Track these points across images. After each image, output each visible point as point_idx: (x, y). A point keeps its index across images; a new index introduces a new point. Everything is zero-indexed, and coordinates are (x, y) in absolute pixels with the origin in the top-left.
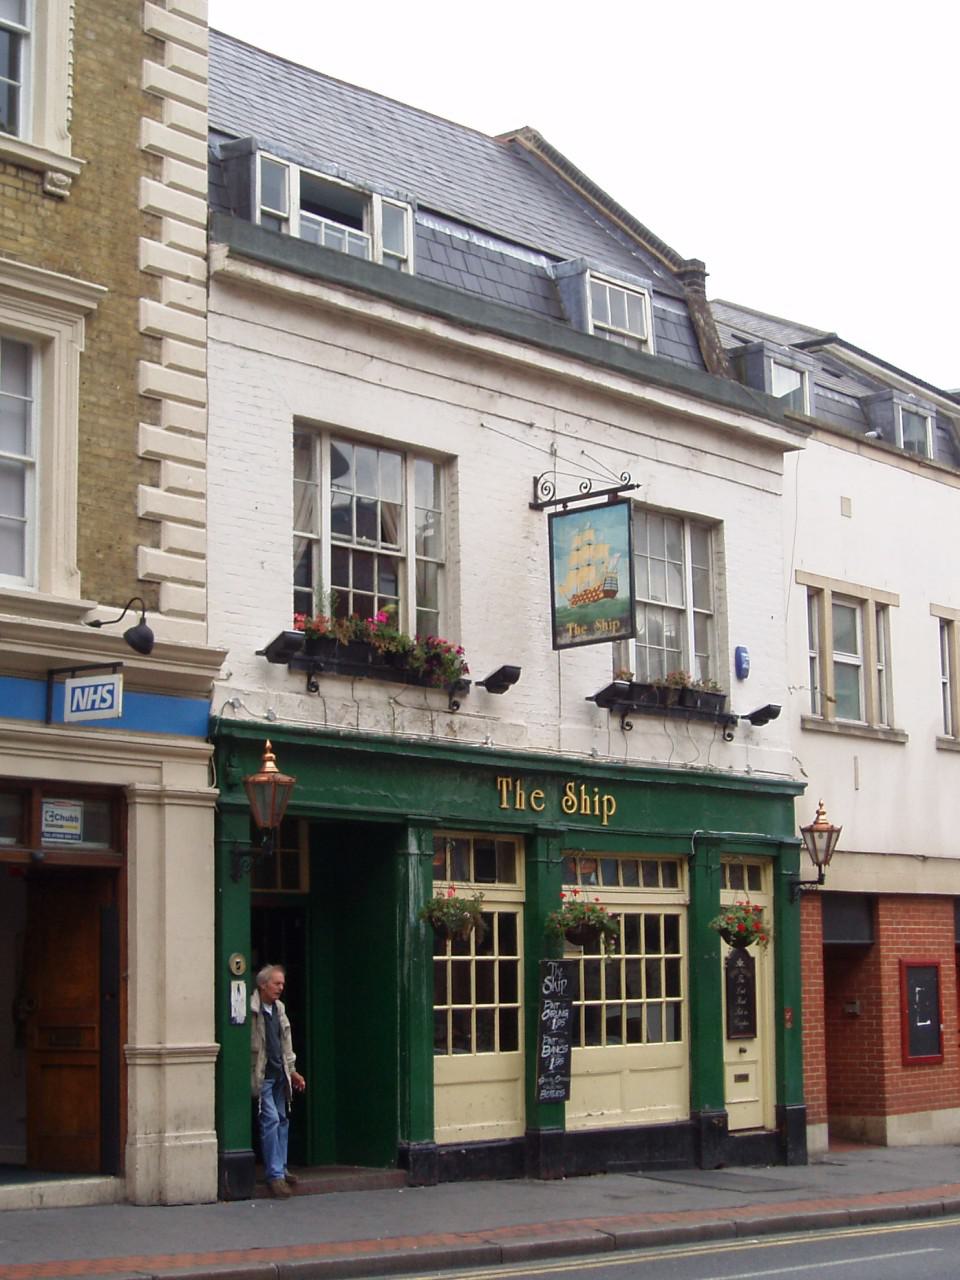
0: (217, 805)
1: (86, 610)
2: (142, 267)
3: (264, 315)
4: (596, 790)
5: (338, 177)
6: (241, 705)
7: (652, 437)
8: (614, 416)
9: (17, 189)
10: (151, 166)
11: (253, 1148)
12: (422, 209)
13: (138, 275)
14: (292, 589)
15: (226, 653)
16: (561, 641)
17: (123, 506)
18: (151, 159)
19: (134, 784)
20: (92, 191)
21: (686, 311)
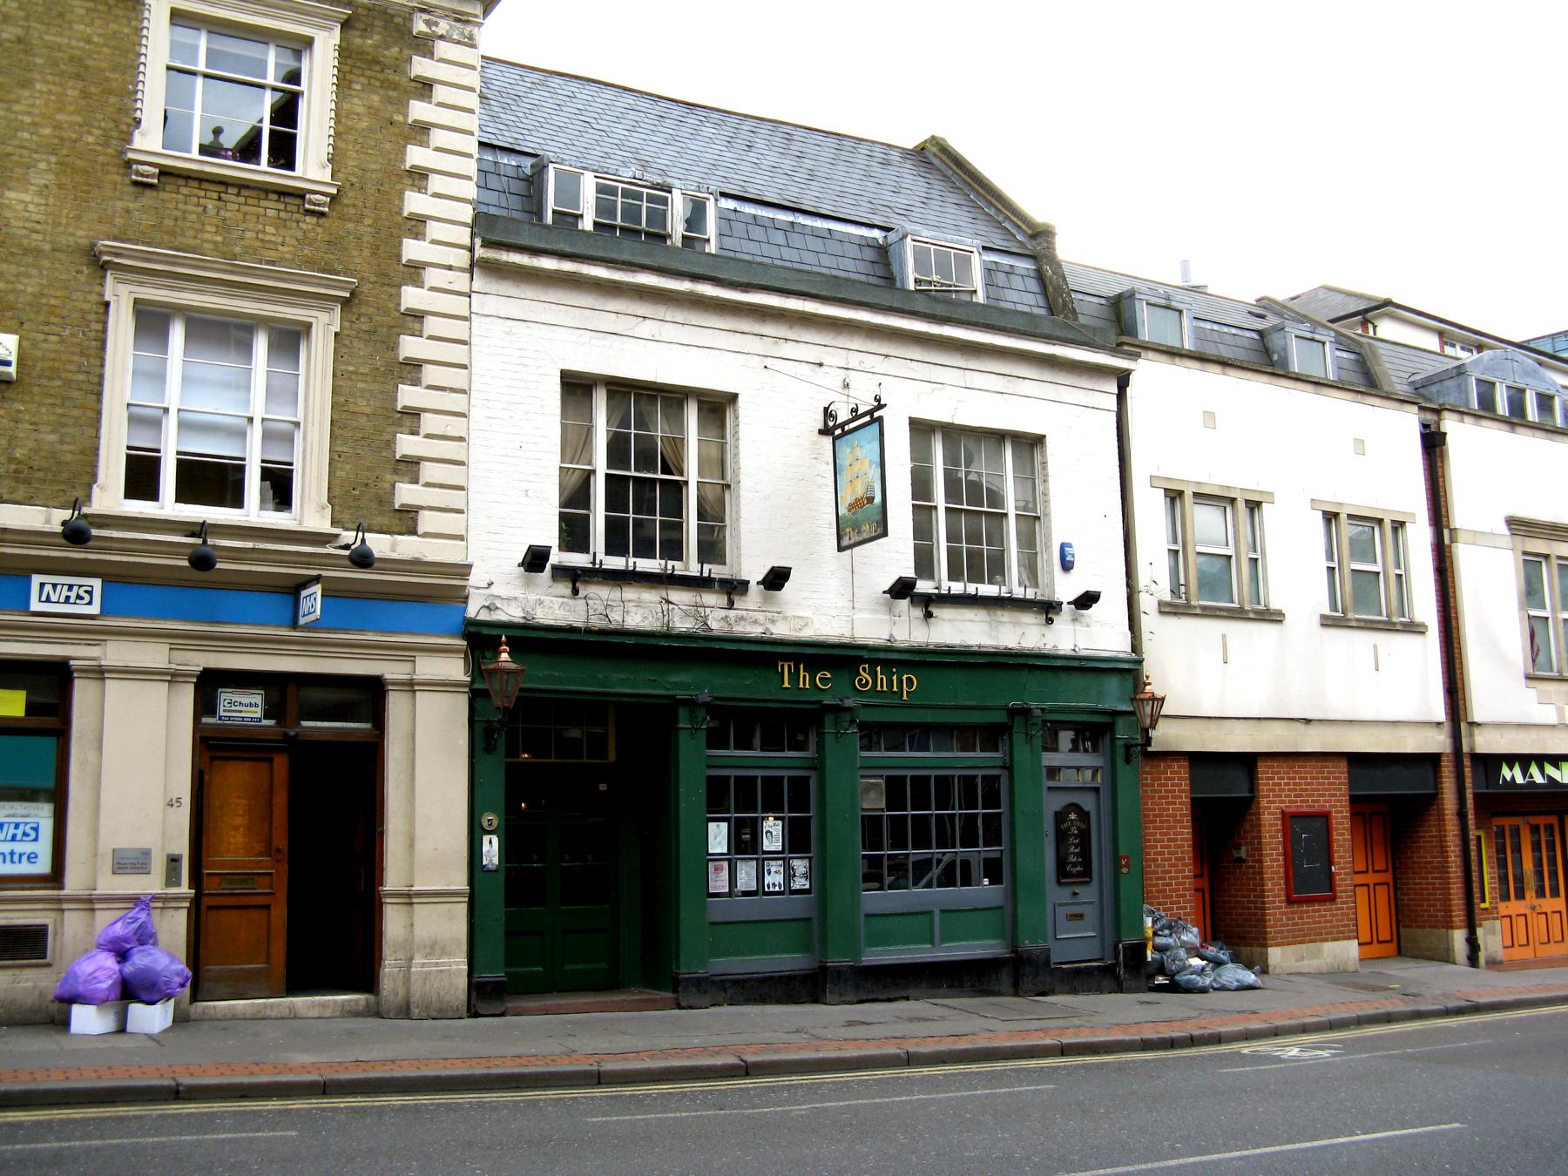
1: (337, 536)
2: (404, 262)
3: (529, 292)
5: (634, 178)
6: (497, 608)
8: (916, 353)
9: (279, 210)
10: (416, 182)
12: (723, 195)
13: (401, 268)
14: (556, 511)
16: (846, 542)
17: (380, 452)
18: (417, 176)
19: (383, 675)
20: (355, 206)
21: (1035, 265)
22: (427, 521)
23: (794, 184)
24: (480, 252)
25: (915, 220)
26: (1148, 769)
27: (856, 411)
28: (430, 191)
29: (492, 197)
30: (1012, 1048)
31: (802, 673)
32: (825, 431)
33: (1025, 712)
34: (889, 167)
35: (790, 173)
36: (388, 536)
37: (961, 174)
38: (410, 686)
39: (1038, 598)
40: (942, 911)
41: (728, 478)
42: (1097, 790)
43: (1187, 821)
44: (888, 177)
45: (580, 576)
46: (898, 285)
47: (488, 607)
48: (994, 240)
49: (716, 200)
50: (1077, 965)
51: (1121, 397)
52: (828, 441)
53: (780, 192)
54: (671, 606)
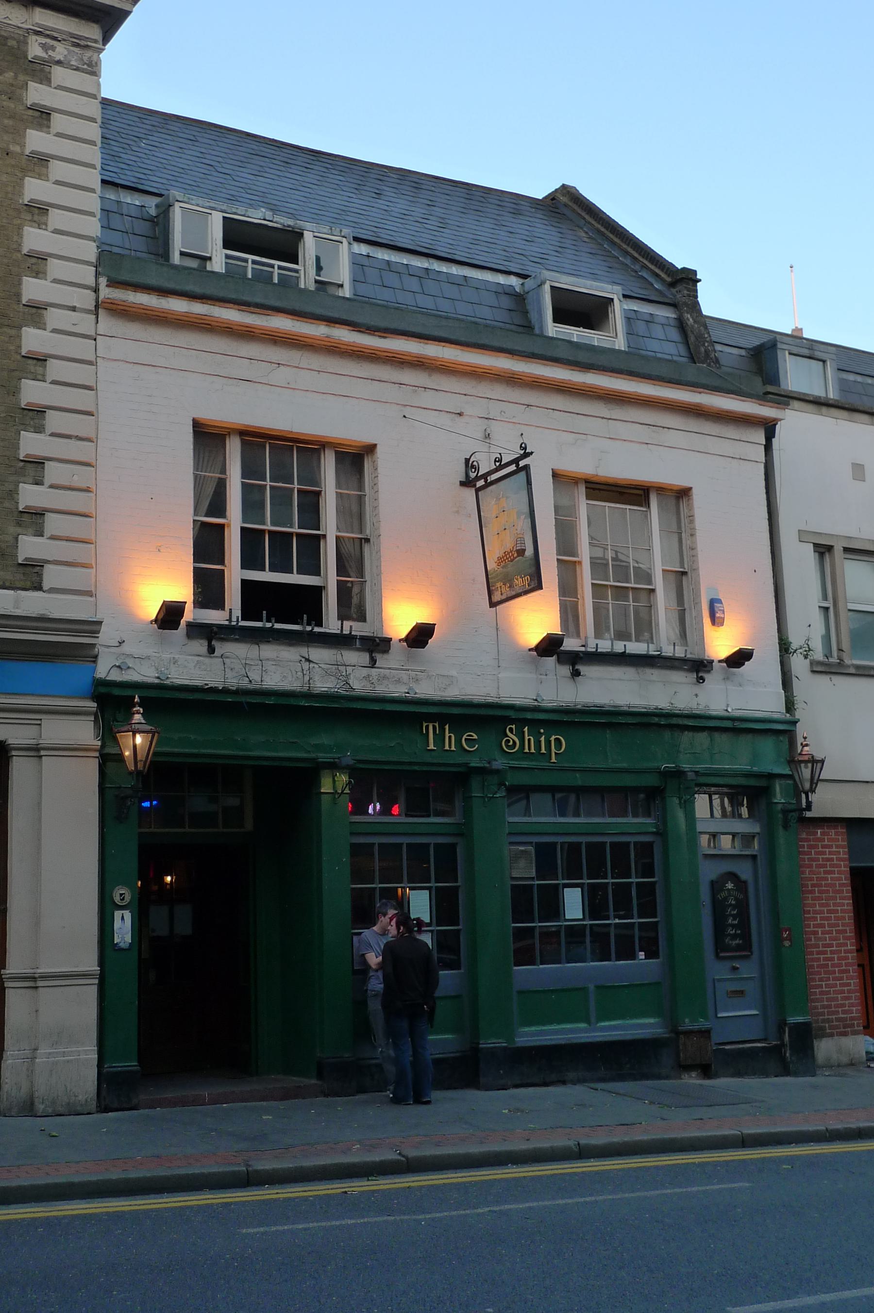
0: (100, 755)
4: (542, 731)
5: (265, 220)
6: (129, 668)
7: (603, 418)
10: (36, 218)
11: (138, 1062)
15: (102, 622)
16: (497, 597)
18: (36, 211)
22: (51, 576)
23: (426, 231)
24: (106, 292)
25: (551, 268)
26: (804, 836)
27: (500, 460)
28: (51, 227)
29: (116, 238)
30: (690, 1139)
31: (447, 735)
32: (467, 483)
33: (678, 774)
34: (521, 217)
35: (421, 220)
36: (12, 592)
37: (593, 222)
38: (36, 751)
39: (689, 656)
40: (598, 987)
41: (368, 532)
42: (754, 857)
43: (847, 892)
44: (521, 226)
45: (216, 633)
46: (537, 331)
47: (119, 667)
48: (633, 289)
49: (350, 244)
50: (741, 1046)
51: (768, 447)
52: (470, 493)
53: (413, 238)
54: (312, 665)
